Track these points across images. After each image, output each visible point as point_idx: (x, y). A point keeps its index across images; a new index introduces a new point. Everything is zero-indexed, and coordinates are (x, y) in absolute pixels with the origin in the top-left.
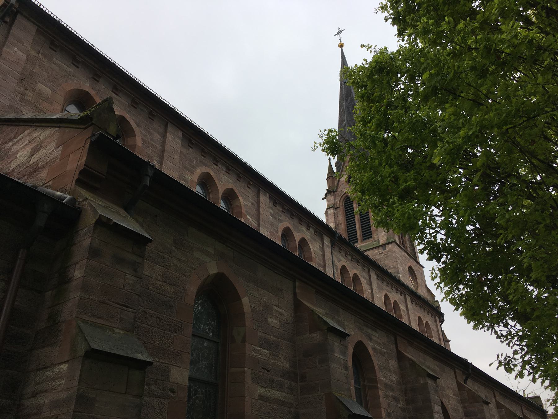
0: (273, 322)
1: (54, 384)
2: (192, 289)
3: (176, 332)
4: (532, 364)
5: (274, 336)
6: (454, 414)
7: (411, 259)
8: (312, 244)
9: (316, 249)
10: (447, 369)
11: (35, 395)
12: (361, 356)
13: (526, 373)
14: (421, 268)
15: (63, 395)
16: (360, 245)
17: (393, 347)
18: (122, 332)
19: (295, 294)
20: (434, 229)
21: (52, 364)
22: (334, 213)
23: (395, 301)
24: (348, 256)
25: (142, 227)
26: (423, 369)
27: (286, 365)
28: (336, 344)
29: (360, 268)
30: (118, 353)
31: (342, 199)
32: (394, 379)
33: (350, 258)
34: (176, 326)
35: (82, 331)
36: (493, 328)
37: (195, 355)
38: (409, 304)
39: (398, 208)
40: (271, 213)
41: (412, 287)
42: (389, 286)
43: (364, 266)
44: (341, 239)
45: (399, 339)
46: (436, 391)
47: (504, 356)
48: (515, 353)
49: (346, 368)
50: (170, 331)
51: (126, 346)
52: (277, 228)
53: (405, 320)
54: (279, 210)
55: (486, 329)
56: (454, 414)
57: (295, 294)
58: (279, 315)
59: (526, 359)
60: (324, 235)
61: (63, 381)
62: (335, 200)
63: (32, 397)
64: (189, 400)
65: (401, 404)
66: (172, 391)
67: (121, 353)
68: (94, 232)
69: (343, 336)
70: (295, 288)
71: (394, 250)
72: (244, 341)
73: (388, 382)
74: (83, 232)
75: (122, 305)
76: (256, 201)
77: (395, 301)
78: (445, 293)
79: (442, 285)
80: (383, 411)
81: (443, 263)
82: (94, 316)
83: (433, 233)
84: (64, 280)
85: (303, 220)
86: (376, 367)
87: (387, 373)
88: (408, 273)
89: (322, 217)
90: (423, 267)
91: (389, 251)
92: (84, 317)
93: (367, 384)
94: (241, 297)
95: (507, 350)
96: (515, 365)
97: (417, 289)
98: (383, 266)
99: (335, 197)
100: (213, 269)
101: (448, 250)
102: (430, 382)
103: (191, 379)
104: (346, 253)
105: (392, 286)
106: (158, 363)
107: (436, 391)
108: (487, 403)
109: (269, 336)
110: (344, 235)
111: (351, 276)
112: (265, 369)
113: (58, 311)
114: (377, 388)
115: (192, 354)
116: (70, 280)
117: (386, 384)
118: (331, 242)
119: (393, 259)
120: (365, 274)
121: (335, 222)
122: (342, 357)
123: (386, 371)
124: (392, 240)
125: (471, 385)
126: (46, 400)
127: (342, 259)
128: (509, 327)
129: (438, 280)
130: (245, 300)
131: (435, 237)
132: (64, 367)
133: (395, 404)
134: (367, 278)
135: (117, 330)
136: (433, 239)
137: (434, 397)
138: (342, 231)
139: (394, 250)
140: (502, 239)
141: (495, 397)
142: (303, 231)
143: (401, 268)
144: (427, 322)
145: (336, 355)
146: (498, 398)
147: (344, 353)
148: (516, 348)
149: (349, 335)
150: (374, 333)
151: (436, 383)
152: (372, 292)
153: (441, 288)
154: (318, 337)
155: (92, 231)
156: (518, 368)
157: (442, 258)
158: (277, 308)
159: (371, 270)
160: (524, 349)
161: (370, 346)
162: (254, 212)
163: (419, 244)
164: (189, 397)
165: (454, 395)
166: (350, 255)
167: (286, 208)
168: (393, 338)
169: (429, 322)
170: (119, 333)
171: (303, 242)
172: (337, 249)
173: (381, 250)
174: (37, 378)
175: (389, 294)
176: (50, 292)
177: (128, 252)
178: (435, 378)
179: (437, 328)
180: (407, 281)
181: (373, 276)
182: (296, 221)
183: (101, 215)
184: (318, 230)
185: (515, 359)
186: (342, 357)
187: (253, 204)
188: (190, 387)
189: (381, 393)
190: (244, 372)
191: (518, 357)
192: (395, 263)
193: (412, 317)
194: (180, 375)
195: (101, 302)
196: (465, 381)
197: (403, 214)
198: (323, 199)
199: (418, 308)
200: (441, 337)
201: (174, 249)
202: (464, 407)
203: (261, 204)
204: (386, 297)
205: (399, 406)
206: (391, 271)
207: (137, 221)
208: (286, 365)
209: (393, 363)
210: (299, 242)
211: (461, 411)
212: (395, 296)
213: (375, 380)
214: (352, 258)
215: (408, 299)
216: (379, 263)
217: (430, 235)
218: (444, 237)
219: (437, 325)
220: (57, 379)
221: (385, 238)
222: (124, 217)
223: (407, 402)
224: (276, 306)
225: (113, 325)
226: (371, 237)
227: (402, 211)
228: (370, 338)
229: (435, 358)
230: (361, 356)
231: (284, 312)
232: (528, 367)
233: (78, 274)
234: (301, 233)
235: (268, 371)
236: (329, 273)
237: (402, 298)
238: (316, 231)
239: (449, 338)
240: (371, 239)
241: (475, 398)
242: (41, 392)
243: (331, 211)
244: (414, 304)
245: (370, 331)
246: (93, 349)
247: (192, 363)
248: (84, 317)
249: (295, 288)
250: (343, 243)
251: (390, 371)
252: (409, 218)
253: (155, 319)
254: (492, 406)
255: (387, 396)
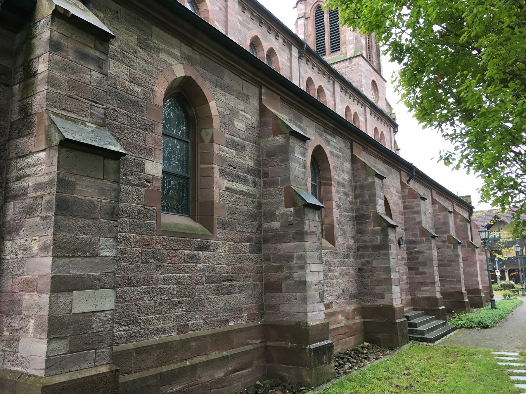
0: (240, 125)
1: (35, 169)
2: (160, 90)
3: (147, 131)
4: (470, 158)
5: (241, 138)
6: (395, 208)
7: (375, 73)
8: (280, 54)
9: (284, 60)
10: (393, 171)
11: (19, 179)
12: (319, 160)
13: (462, 165)
14: (384, 82)
15: (45, 179)
16: (328, 58)
17: (348, 152)
18: (94, 126)
19: (261, 100)
20: (400, 28)
21: (30, 152)
22: (304, 24)
23: (355, 113)
24: (315, 68)
25: (104, 23)
26: (372, 170)
27: (251, 163)
28: (297, 146)
29: (326, 80)
30: (92, 144)
31: (313, 8)
32: (347, 178)
33: (316, 69)
34: (147, 124)
35: (54, 123)
36: (440, 127)
37: (167, 152)
38: (368, 115)
39: (367, 4)
40: (239, 20)
41: (373, 101)
42: (352, 98)
43: (330, 79)
44: (309, 50)
45: (354, 143)
46: (382, 188)
47: (446, 152)
48: (456, 148)
49: (305, 167)
50: (141, 129)
51: (99, 138)
52: (246, 37)
53: (363, 129)
54: (247, 16)
55: (434, 127)
56: (395, 208)
57: (261, 100)
58: (245, 119)
59: (465, 153)
60: (292, 46)
61: (43, 167)
62: (306, 9)
63: (17, 181)
64: (164, 190)
65: (350, 198)
66: (148, 181)
67: (95, 144)
68: (52, 24)
69: (304, 139)
70: (261, 94)
71: (360, 63)
72: (212, 141)
73: (341, 181)
74: (41, 24)
75: (91, 101)
76: (224, 5)
77: (355, 113)
78: (401, 96)
79: (401, 87)
80: (334, 204)
81: (405, 64)
82: (64, 109)
83: (399, 33)
84: (30, 74)
85: (271, 28)
86: (332, 168)
87: (341, 173)
88: (371, 87)
89: (292, 28)
90: (386, 81)
91: (355, 65)
92: (55, 110)
93: (322, 181)
94: (209, 101)
95: (449, 146)
96: (454, 160)
97: (377, 102)
98: (348, 79)
99: (306, 6)
100: (180, 72)
101: (410, 50)
102: (377, 180)
103: (163, 172)
104: (313, 65)
105: (354, 99)
106: (133, 157)
107: (382, 188)
108: (424, 199)
109: (236, 138)
110: (313, 47)
111: (317, 87)
112: (232, 166)
113: (28, 104)
114: (331, 185)
115: (164, 152)
116: (35, 74)
117: (338, 182)
118: (299, 52)
119: (359, 74)
120: (330, 87)
121: (305, 33)
122: (301, 157)
123: (340, 171)
124: (359, 53)
125: (413, 185)
126: (30, 182)
127: (308, 69)
128: (455, 125)
129: (396, 83)
130: (212, 104)
131: (400, 38)
132: (43, 155)
133: (344, 198)
134: (332, 90)
135: (88, 124)
136: (398, 40)
137: (379, 193)
138: (311, 43)
139: (360, 63)
140: (465, 37)
141: (432, 195)
142: (271, 40)
143: (364, 82)
144: (382, 132)
145: (296, 155)
146: (434, 196)
147: (304, 154)
148: (458, 144)
149: (309, 139)
150: (333, 139)
151: (382, 182)
152: (335, 103)
153: (398, 91)
154: (281, 140)
155: (50, 23)
156: (455, 163)
157: (403, 59)
158: (243, 113)
159: (335, 82)
160: (464, 146)
161: (327, 149)
162: (222, 18)
163: (384, 44)
164: (164, 188)
165: (397, 192)
166: (317, 67)
167: (255, 14)
168: (349, 144)
169: (384, 133)
170: (90, 126)
171: (271, 53)
172: (304, 60)
173: (347, 63)
174: (19, 165)
175: (350, 107)
176: (17, 86)
177: (91, 47)
178: (382, 178)
179: (391, 138)
180: (369, 94)
181: (337, 87)
182: (265, 29)
183: (56, 5)
184: (286, 40)
185: (455, 154)
186: (301, 157)
187: (221, 9)
188: (164, 179)
189: (334, 189)
190: (213, 168)
191: (458, 152)
192: (359, 77)
193: (369, 127)
194: (154, 168)
195: (69, 96)
196: (408, 182)
197: (371, 12)
198: (294, 8)
199: (376, 119)
200: (393, 146)
201: (139, 49)
202: (404, 202)
203: (229, 9)
204: (348, 108)
205: (349, 199)
206: (355, 85)
207: (97, 16)
208: (251, 163)
209: (347, 165)
210: (268, 52)
211: (401, 205)
212: (356, 108)
213: (330, 179)
214: (319, 70)
215: (368, 110)
216: (345, 77)
217: (396, 34)
218: (409, 38)
219: (391, 135)
220: (37, 165)
221: (353, 51)
222: (83, 10)
223: (356, 197)
224: (242, 111)
225: (84, 119)
226: (339, 50)
227: (371, 7)
228: (328, 143)
229: (385, 162)
230: (319, 160)
231: (249, 117)
232: (465, 161)
233: (42, 67)
234: (270, 42)
235: (234, 168)
236: (295, 82)
237: (362, 110)
238: (284, 41)
239: (399, 147)
240: (339, 52)
241: (413, 195)
242: (24, 176)
243: (301, 21)
244: (373, 115)
245: (329, 137)
246: (66, 139)
247: (164, 159)
248: (55, 110)
249: (261, 94)
250: (312, 55)
251: (343, 171)
252: (377, 15)
253: (126, 117)
254: (428, 201)
255: (338, 192)
